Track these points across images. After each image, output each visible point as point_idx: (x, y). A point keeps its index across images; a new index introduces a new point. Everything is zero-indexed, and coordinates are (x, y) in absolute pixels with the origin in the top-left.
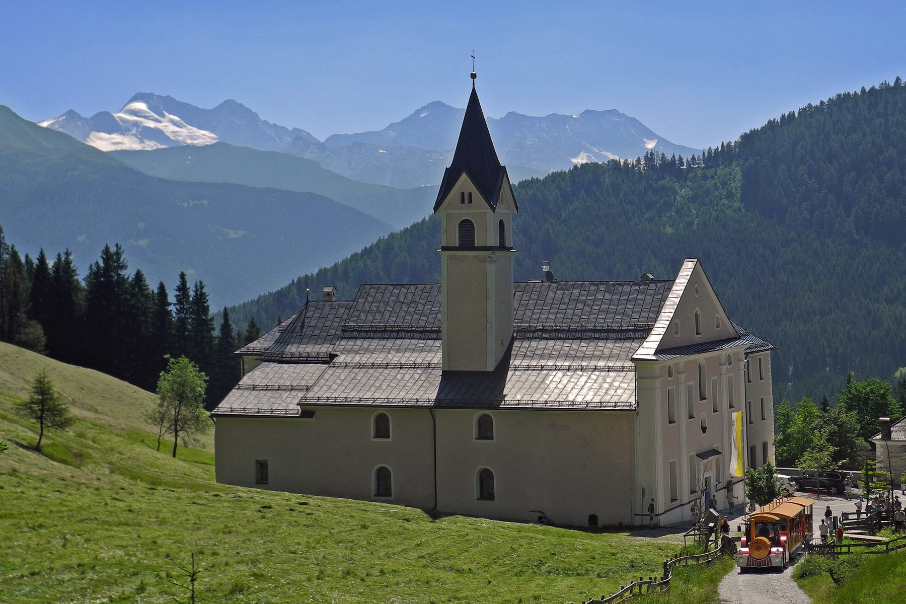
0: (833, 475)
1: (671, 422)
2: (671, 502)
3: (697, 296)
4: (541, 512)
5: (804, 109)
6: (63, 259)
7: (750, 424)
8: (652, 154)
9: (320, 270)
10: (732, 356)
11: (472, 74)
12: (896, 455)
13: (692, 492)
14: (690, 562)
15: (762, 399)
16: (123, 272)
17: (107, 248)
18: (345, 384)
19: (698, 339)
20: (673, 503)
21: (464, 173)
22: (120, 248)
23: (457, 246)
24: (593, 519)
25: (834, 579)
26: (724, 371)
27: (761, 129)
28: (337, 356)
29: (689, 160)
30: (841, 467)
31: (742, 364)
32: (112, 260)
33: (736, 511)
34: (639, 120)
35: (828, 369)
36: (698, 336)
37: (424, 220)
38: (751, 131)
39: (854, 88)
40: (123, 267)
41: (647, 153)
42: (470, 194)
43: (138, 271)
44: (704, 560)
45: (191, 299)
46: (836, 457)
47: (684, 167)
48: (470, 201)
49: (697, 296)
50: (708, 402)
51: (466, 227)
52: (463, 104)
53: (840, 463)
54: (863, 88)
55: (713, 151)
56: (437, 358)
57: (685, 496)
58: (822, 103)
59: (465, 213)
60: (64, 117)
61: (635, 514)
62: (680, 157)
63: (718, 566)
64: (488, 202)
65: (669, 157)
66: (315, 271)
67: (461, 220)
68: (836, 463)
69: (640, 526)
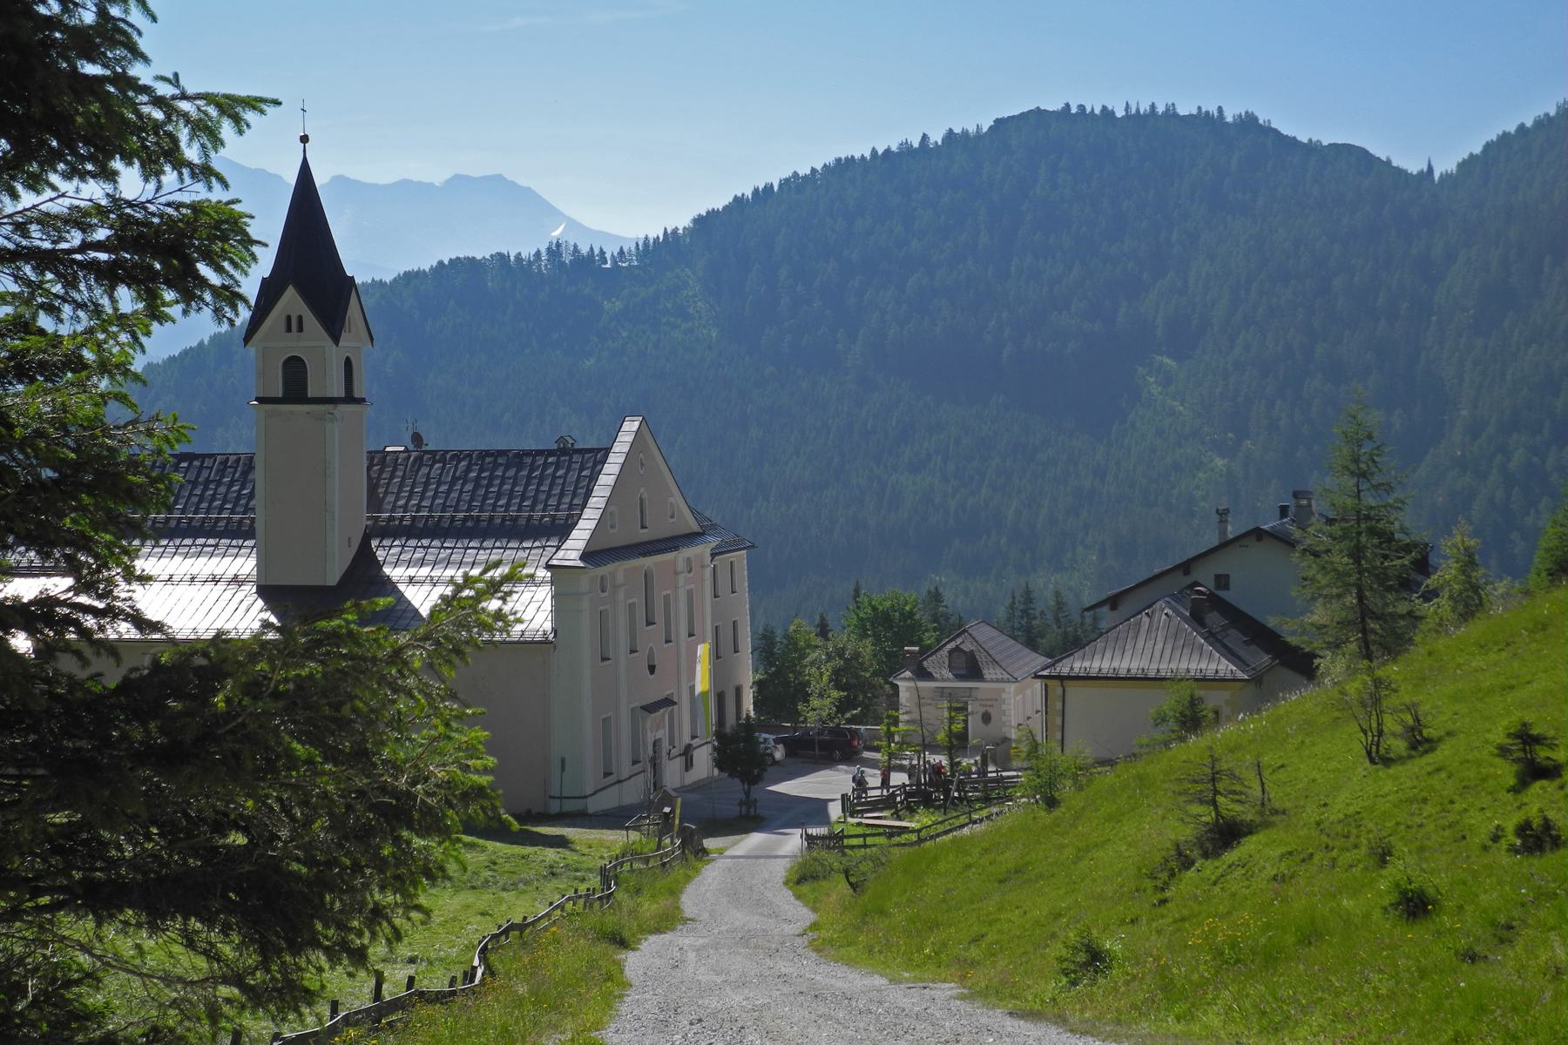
0: (838, 731)
1: (604, 659)
3: (642, 472)
5: (787, 180)
8: (558, 245)
12: (929, 701)
13: (635, 762)
14: (636, 865)
15: (734, 622)
19: (645, 535)
20: (607, 779)
21: (291, 287)
23: (280, 395)
25: (851, 884)
27: (724, 208)
29: (615, 254)
30: (849, 721)
31: (708, 573)
33: (1150, 828)
35: (158, 266)
37: (201, 344)
38: (708, 212)
39: (861, 150)
41: (551, 243)
42: (300, 319)
44: (656, 862)
46: (842, 707)
47: (608, 266)
48: (300, 329)
50: (658, 629)
51: (295, 371)
52: (291, 177)
53: (848, 715)
54: (874, 149)
55: (652, 241)
56: (246, 565)
57: (626, 769)
58: (813, 170)
61: (551, 797)
62: (601, 249)
63: (678, 872)
65: (584, 250)
67: (286, 357)
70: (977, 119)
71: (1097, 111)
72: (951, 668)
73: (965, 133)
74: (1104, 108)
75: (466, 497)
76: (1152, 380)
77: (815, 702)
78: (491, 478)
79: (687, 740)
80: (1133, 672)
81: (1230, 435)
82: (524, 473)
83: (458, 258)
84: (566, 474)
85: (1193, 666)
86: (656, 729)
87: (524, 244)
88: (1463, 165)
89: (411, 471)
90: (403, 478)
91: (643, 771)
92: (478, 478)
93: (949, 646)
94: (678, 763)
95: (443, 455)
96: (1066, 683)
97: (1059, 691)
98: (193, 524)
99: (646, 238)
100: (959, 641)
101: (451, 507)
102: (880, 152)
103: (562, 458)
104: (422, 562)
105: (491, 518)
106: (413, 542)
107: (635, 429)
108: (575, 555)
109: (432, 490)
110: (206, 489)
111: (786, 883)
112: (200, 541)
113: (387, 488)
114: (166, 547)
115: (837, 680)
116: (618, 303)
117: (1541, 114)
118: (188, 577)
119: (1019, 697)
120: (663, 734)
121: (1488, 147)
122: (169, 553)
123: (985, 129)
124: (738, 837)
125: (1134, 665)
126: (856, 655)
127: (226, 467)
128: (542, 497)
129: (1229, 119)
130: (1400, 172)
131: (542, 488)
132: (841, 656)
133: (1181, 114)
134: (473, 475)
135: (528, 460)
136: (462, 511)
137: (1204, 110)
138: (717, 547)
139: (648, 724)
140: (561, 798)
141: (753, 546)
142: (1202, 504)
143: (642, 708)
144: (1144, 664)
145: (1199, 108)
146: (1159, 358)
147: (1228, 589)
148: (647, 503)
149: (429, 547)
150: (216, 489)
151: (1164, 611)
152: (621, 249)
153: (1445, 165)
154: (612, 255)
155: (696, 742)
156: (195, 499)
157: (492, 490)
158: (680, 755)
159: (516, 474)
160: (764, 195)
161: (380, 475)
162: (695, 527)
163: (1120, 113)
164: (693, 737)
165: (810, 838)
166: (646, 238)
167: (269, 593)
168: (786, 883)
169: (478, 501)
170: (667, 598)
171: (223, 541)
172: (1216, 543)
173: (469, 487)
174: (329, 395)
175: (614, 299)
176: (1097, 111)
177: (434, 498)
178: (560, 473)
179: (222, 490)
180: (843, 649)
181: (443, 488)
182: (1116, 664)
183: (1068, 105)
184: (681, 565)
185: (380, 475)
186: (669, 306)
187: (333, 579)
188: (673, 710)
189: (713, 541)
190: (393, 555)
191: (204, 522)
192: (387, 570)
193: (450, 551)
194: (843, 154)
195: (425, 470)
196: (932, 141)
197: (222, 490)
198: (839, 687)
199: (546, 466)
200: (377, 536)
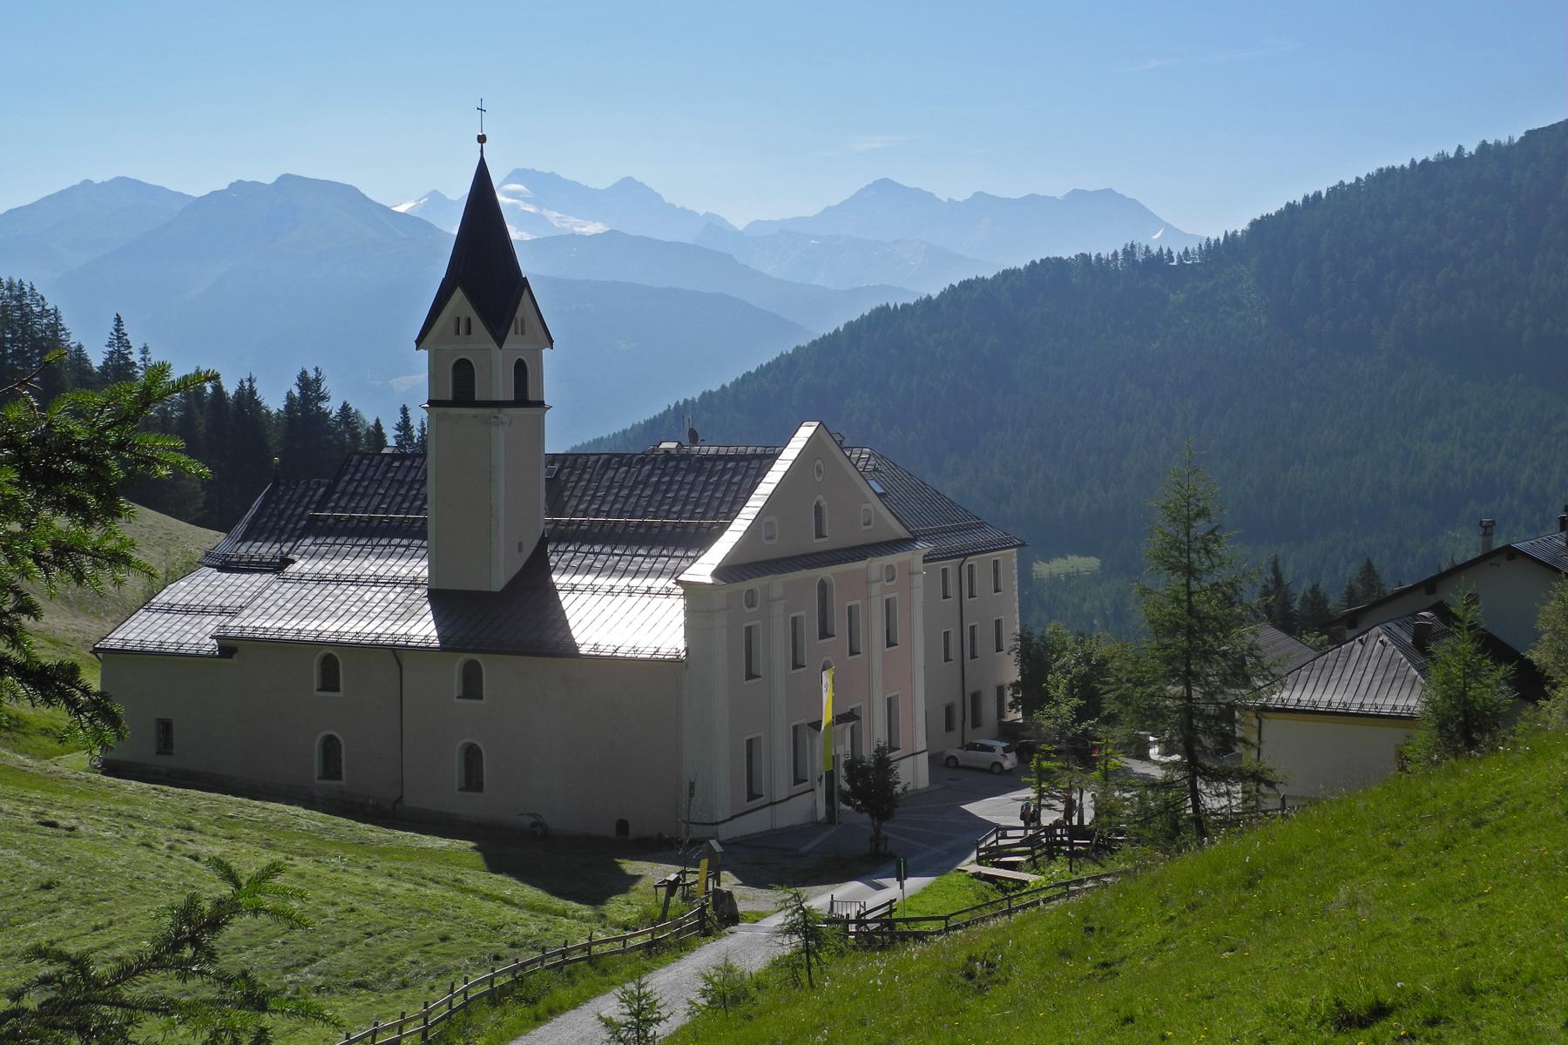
2: (748, 801)
5: (1334, 189)
9: (704, 393)
11: (479, 136)
16: (324, 405)
17: (304, 373)
18: (289, 606)
21: (458, 288)
22: (321, 374)
23: (450, 397)
24: (622, 826)
28: (293, 562)
29: (1181, 254)
32: (310, 387)
34: (18, 206)
37: (837, 331)
39: (1401, 160)
40: (324, 398)
42: (469, 320)
43: (345, 403)
45: (415, 441)
47: (1175, 263)
48: (469, 332)
49: (819, 479)
54: (1413, 160)
55: (1213, 243)
56: (419, 568)
58: (1358, 179)
60: (426, 199)
62: (1169, 250)
64: (492, 332)
66: (697, 396)
67: (455, 360)
70: (1510, 131)
73: (1498, 144)
75: (643, 502)
78: (670, 483)
80: (1334, 706)
82: (703, 478)
83: (1048, 258)
87: (1105, 244)
89: (598, 474)
90: (589, 481)
91: (813, 790)
95: (630, 458)
98: (393, 524)
99: (1208, 239)
102: (1418, 162)
103: (741, 464)
106: (585, 548)
112: (396, 541)
113: (572, 492)
114: (364, 546)
116: (1182, 295)
123: (1516, 141)
125: (1337, 699)
128: (716, 503)
132: (1088, 662)
134: (655, 479)
135: (708, 465)
138: (929, 554)
141: (1023, 545)
143: (809, 724)
144: (1347, 698)
148: (826, 512)
149: (600, 553)
152: (1186, 249)
154: (1179, 254)
156: (399, 499)
157: (669, 495)
159: (695, 479)
160: (1313, 201)
161: (568, 477)
165: (807, 928)
166: (1208, 239)
167: (442, 600)
169: (654, 507)
173: (648, 492)
174: (495, 398)
175: (1178, 292)
177: (614, 502)
178: (737, 479)
181: (624, 492)
184: (874, 575)
185: (568, 477)
186: (1226, 297)
187: (498, 582)
189: (923, 547)
190: (565, 561)
194: (1385, 164)
195: (610, 473)
196: (1467, 151)
199: (724, 471)
200: (555, 540)
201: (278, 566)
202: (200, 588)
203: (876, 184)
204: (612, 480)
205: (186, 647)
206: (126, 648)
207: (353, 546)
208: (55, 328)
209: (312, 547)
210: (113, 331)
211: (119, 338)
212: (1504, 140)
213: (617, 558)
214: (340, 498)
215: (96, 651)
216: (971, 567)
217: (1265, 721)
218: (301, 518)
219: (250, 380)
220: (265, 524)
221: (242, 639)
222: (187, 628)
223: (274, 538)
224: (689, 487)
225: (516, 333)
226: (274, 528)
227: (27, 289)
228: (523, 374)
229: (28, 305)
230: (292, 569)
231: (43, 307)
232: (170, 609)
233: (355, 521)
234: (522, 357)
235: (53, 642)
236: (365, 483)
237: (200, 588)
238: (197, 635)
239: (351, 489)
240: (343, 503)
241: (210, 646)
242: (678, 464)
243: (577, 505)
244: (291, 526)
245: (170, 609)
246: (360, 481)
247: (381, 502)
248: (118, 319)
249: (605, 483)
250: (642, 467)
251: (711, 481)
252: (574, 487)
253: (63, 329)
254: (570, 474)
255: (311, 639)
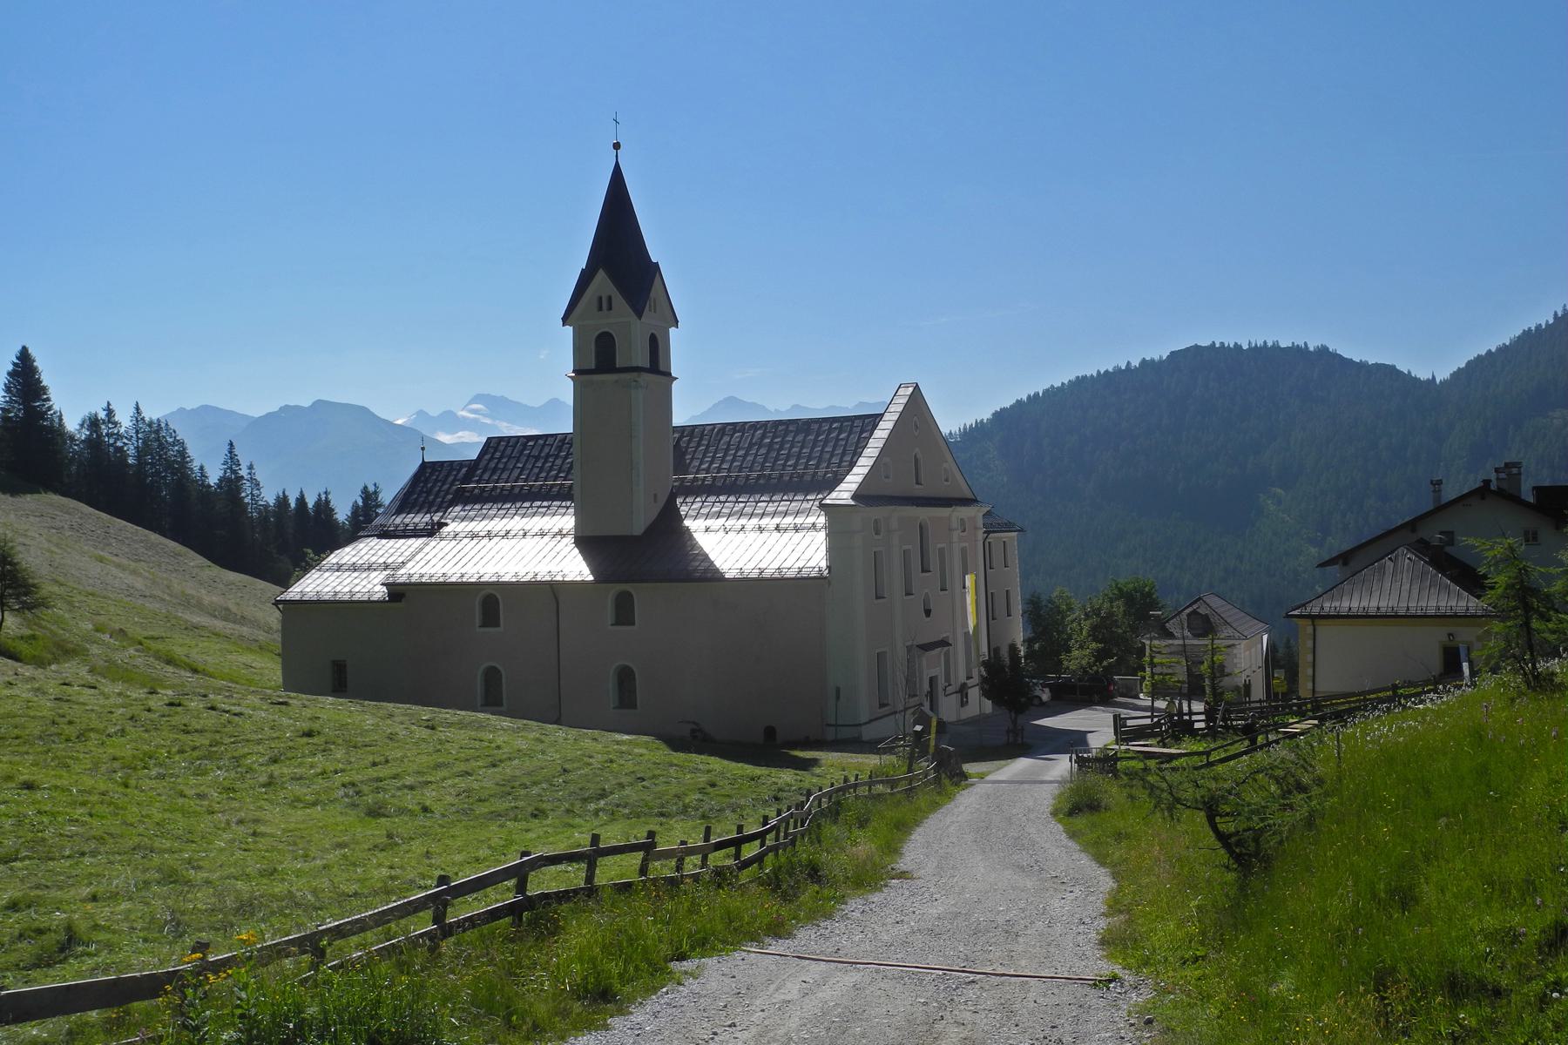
4: (694, 723)
5: (1047, 390)
6: (323, 499)
7: (993, 619)
10: (966, 520)
11: (614, 144)
15: (1007, 591)
17: (366, 487)
19: (919, 491)
23: (593, 367)
26: (955, 539)
28: (446, 525)
36: (917, 486)
39: (1091, 371)
42: (610, 298)
46: (1100, 656)
48: (610, 308)
56: (568, 522)
58: (1063, 384)
59: (605, 323)
68: (1101, 664)
69: (833, 741)
70: (1160, 352)
71: (1231, 346)
72: (1190, 628)
74: (1236, 344)
76: (1269, 502)
77: (1076, 653)
79: (962, 678)
80: (1383, 610)
81: (1319, 534)
82: (811, 437)
84: (848, 436)
85: (1442, 604)
86: (931, 666)
88: (1454, 375)
90: (708, 446)
92: (772, 442)
93: (1188, 611)
94: (955, 699)
96: (1317, 622)
97: (1310, 630)
100: (1195, 607)
101: (747, 468)
103: (846, 424)
104: (718, 515)
105: (781, 476)
106: (712, 499)
107: (909, 393)
108: (847, 495)
109: (731, 454)
110: (546, 461)
111: (1054, 814)
114: (509, 509)
115: (1095, 633)
117: (1501, 344)
118: (521, 533)
119: (1247, 653)
120: (938, 671)
121: (1469, 363)
122: (510, 514)
123: (1164, 358)
124: (1003, 762)
126: (1110, 614)
127: (564, 444)
129: (1312, 349)
130: (1416, 380)
131: (827, 449)
132: (1098, 615)
133: (1282, 346)
136: (756, 472)
137: (1296, 344)
139: (924, 662)
140: (836, 725)
142: (1303, 575)
145: (1293, 343)
146: (1274, 489)
147: (1453, 545)
150: (554, 462)
151: (1406, 558)
153: (1443, 375)
155: (970, 683)
156: (536, 470)
158: (956, 692)
160: (1034, 399)
162: (969, 496)
163: (1245, 347)
164: (968, 678)
167: (586, 543)
168: (1054, 814)
170: (941, 551)
171: (554, 503)
172: (1431, 507)
173: (763, 451)
176: (1231, 346)
178: (842, 436)
179: (559, 462)
180: (1099, 609)
181: (741, 453)
182: (1364, 604)
183: (1214, 342)
184: (955, 524)
187: (639, 527)
188: (948, 651)
191: (541, 488)
192: (687, 523)
193: (743, 505)
195: (726, 439)
196: (1133, 365)
197: (559, 462)
198: (1095, 640)
199: (830, 430)
200: (682, 494)
201: (432, 531)
202: (363, 552)
203: (726, 399)
204: (729, 444)
205: (359, 595)
206: (304, 599)
207: (499, 510)
208: (183, 453)
209: (462, 513)
210: (227, 453)
211: (231, 458)
212: (1157, 358)
213: (742, 505)
214: (483, 473)
215: (277, 603)
216: (989, 543)
217: (1320, 630)
218: (447, 493)
219: (326, 493)
220: (416, 499)
221: (411, 584)
222: (356, 581)
223: (425, 510)
224: (799, 445)
225: (650, 310)
226: (424, 502)
227: (163, 425)
228: (657, 350)
229: (164, 437)
230: (445, 530)
231: (175, 437)
232: (339, 568)
233: (498, 491)
234: (654, 331)
235: (215, 634)
236: (504, 460)
237: (363, 552)
238: (372, 586)
239: (492, 465)
240: (486, 477)
241: (380, 592)
242: (788, 427)
243: (700, 465)
244: (440, 500)
245: (339, 568)
246: (500, 459)
247: (520, 474)
248: (231, 444)
249: (723, 445)
250: (755, 431)
251: (820, 438)
252: (695, 451)
253: (189, 457)
254: (689, 442)
255: (474, 580)
